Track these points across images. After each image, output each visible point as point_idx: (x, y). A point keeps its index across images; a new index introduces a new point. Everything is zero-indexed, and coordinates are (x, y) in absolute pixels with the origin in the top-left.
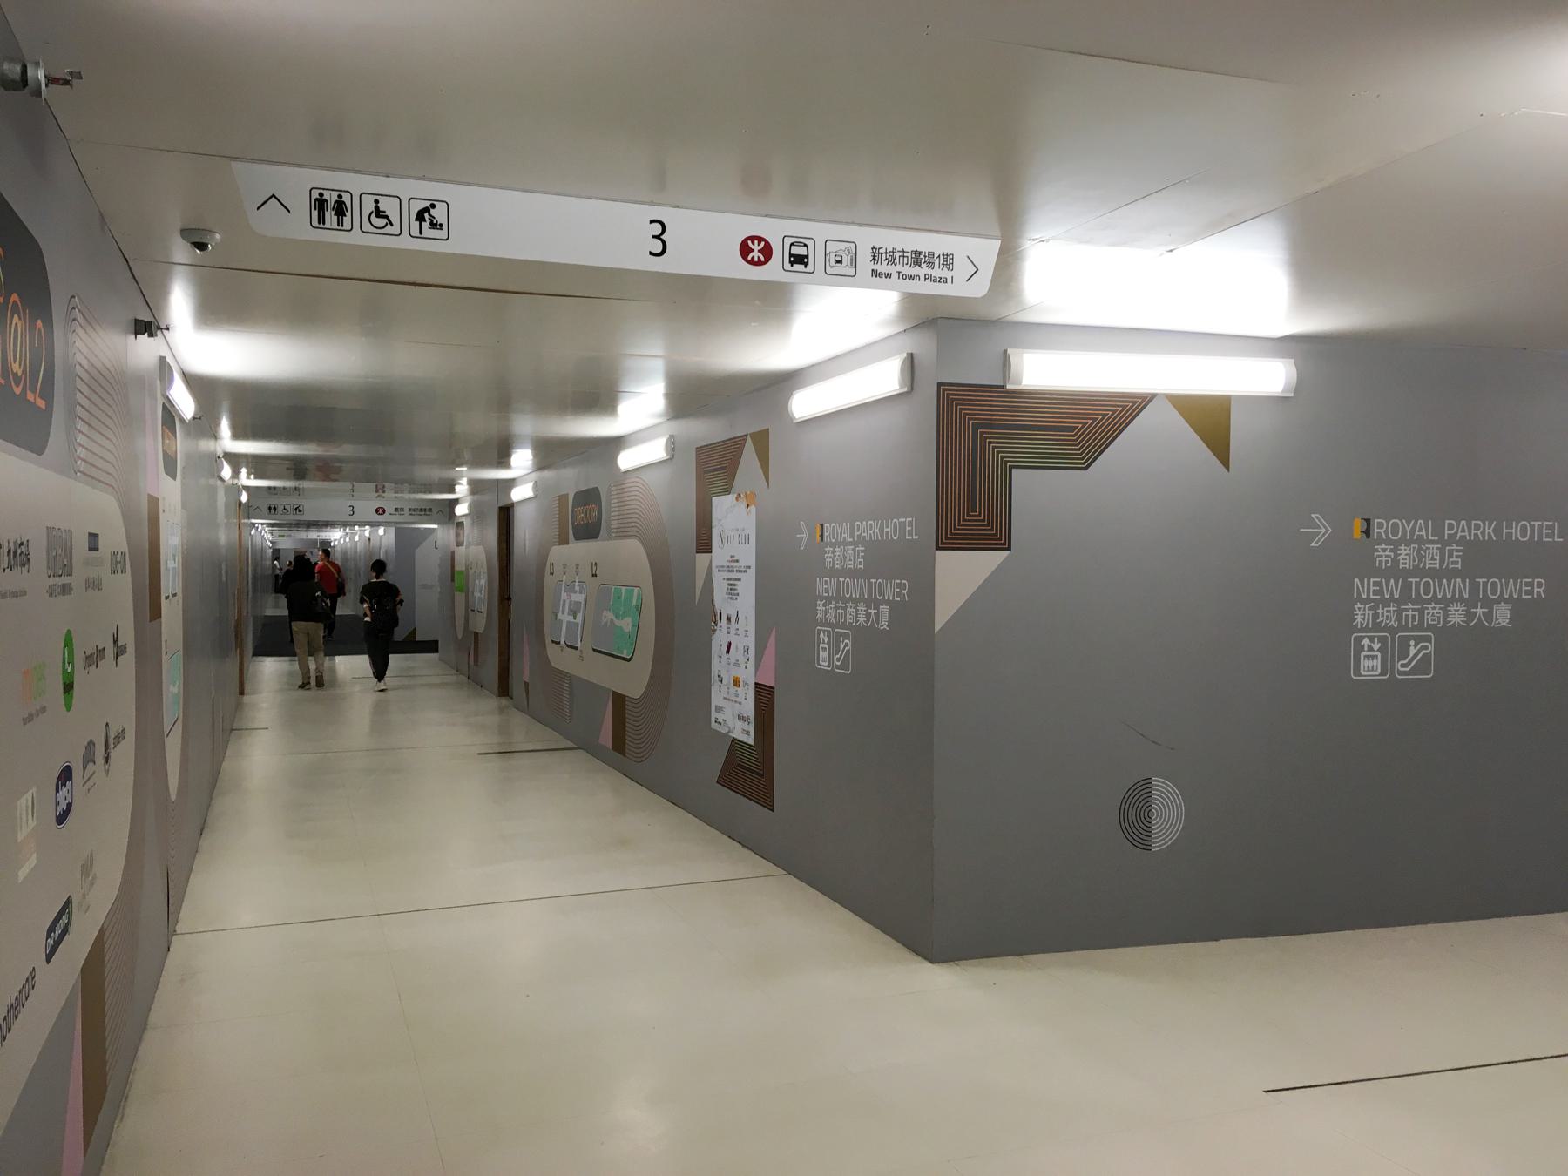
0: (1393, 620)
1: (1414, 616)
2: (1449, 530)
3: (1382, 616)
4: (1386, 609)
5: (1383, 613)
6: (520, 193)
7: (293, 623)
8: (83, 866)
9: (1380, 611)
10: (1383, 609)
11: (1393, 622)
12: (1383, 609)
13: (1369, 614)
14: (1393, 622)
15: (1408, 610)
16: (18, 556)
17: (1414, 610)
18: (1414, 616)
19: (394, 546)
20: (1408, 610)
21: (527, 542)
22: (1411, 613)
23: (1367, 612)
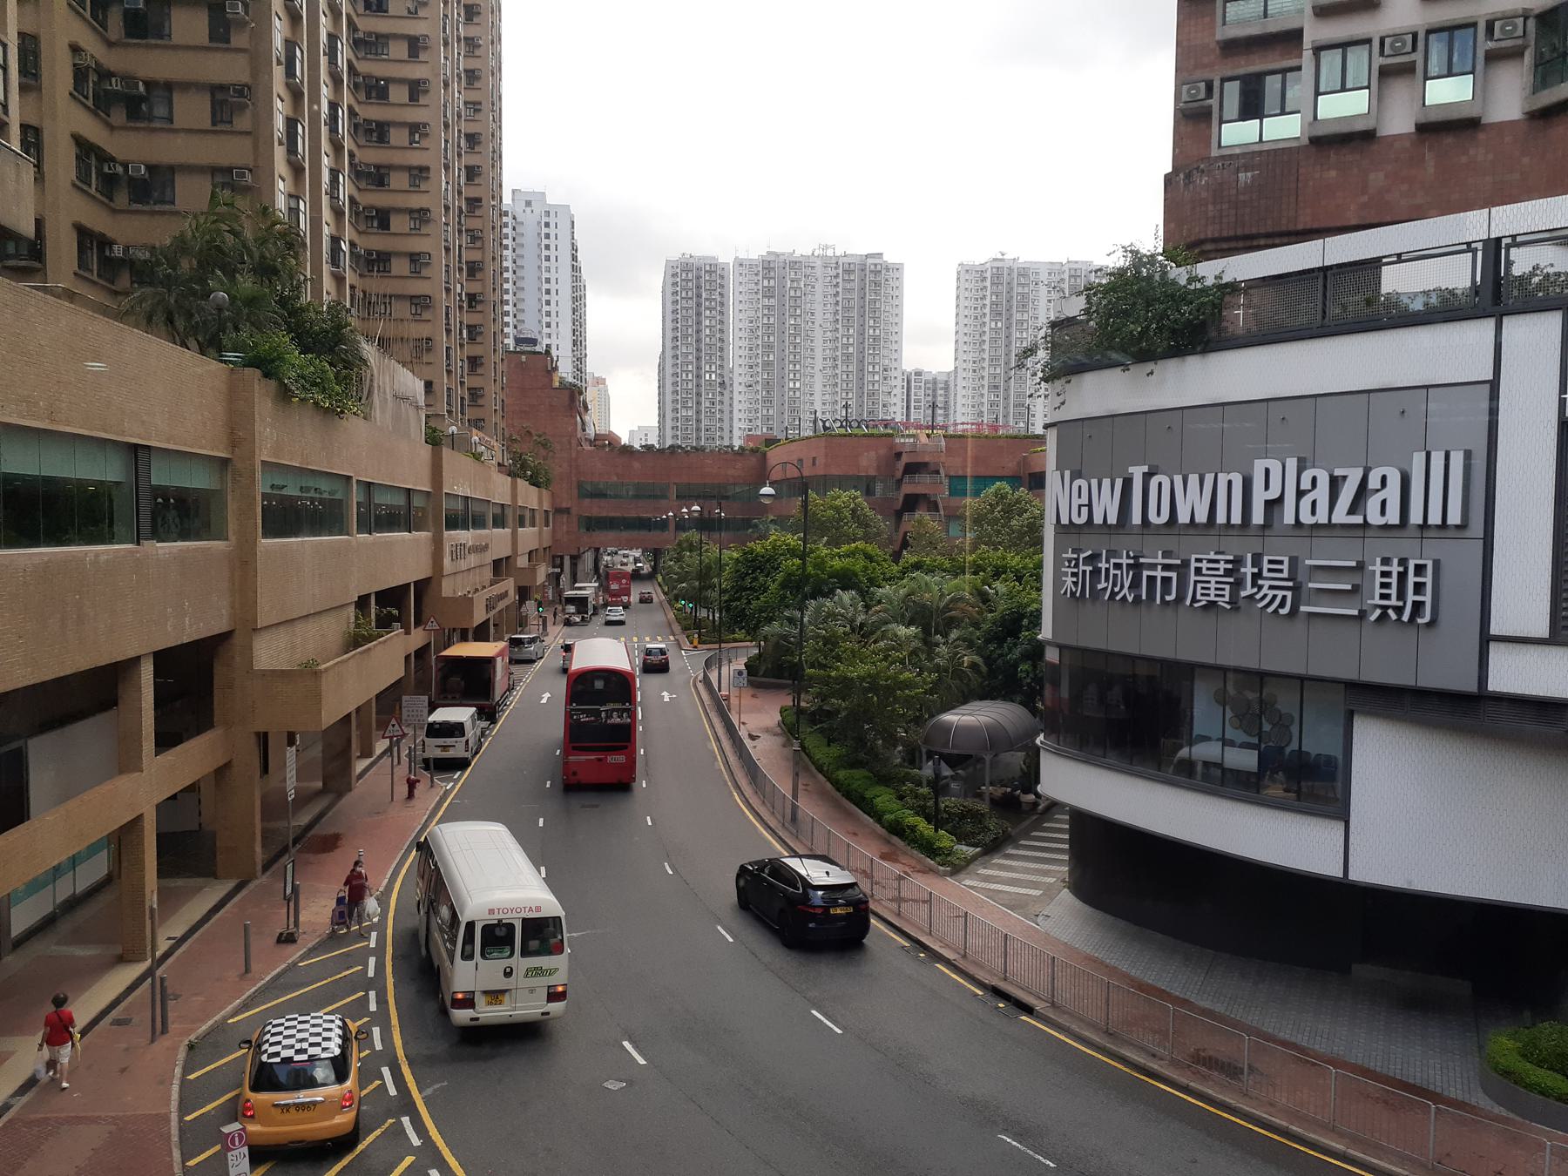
0: (1127, 585)
1: (1167, 581)
2: (1416, 574)
3: (1107, 579)
4: (1112, 561)
5: (1107, 570)
6: (1481, 555)
7: (1228, 4)
8: (1557, 1100)
9: (1103, 565)
10: (1108, 561)
11: (1126, 590)
12: (1108, 561)
13: (1084, 572)
14: (1126, 590)
15: (1153, 567)
16: (471, 13)
17: (1166, 567)
18: (1167, 581)
19: (232, 30)
20: (1153, 567)
21: (1124, 967)
22: (1159, 573)
23: (1082, 568)
